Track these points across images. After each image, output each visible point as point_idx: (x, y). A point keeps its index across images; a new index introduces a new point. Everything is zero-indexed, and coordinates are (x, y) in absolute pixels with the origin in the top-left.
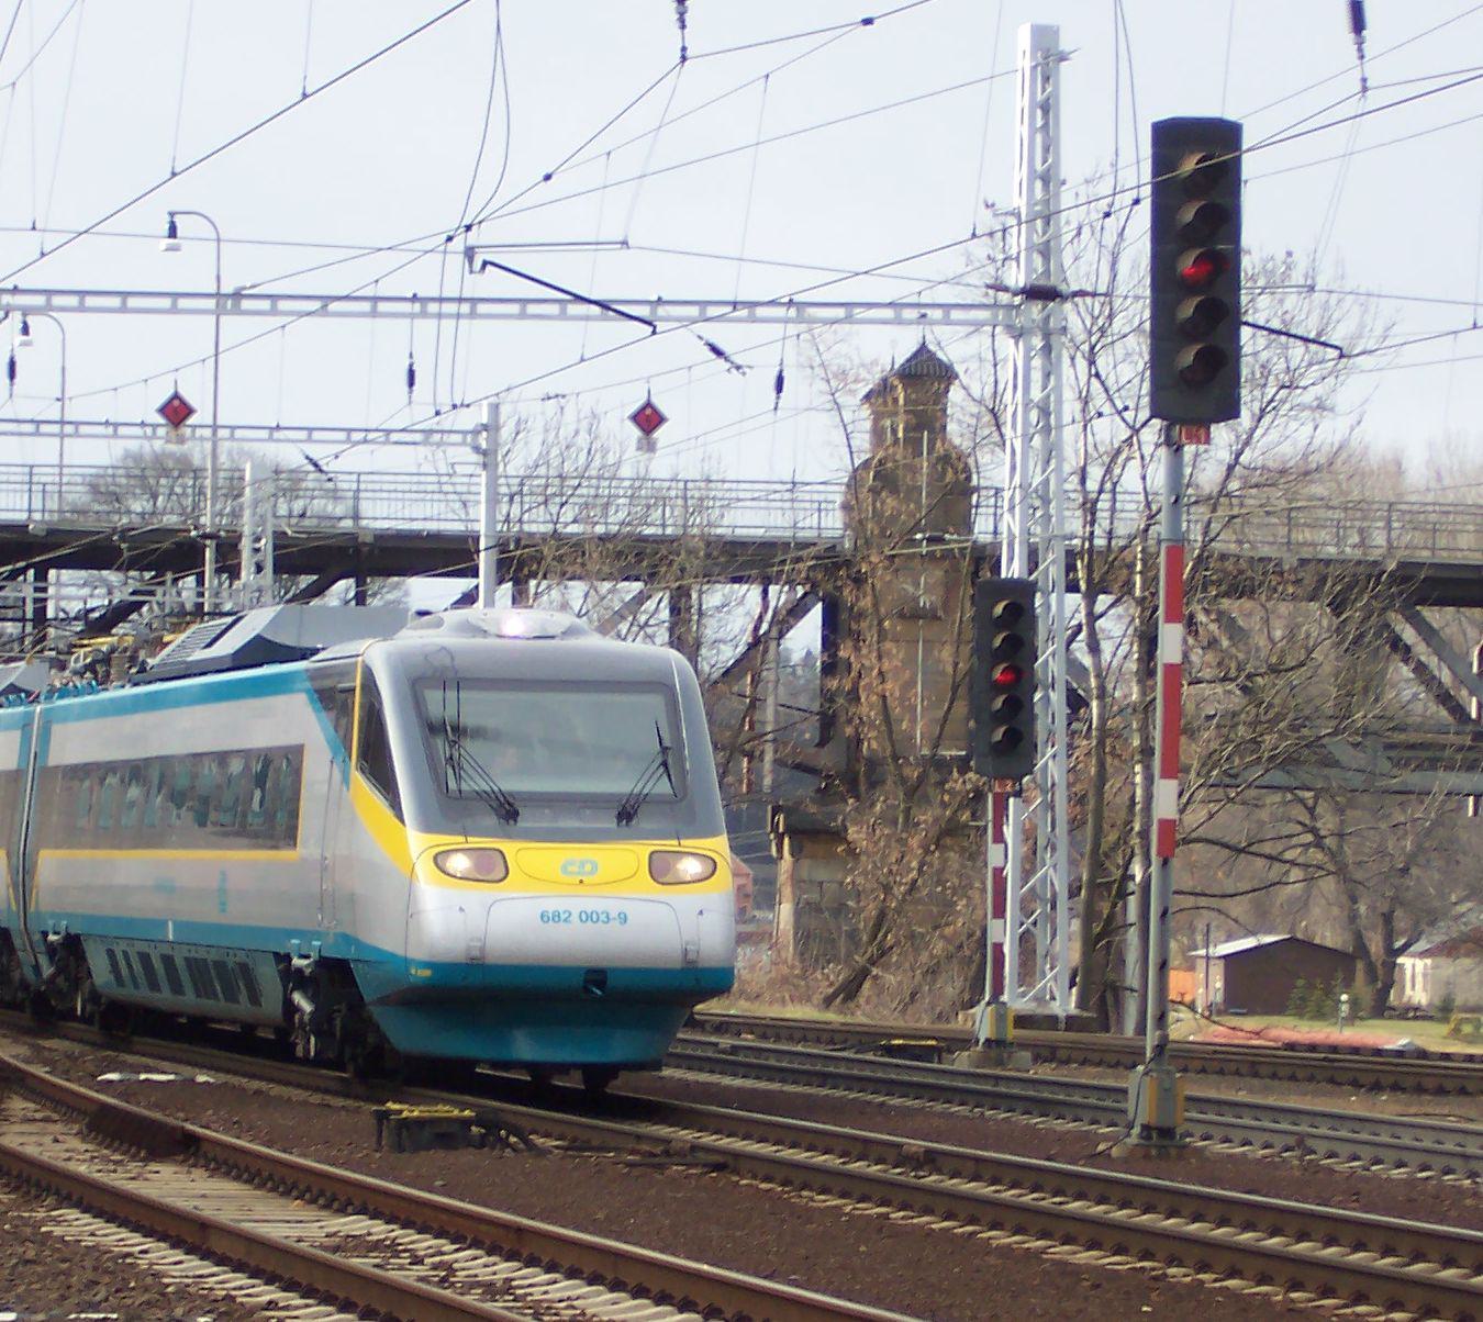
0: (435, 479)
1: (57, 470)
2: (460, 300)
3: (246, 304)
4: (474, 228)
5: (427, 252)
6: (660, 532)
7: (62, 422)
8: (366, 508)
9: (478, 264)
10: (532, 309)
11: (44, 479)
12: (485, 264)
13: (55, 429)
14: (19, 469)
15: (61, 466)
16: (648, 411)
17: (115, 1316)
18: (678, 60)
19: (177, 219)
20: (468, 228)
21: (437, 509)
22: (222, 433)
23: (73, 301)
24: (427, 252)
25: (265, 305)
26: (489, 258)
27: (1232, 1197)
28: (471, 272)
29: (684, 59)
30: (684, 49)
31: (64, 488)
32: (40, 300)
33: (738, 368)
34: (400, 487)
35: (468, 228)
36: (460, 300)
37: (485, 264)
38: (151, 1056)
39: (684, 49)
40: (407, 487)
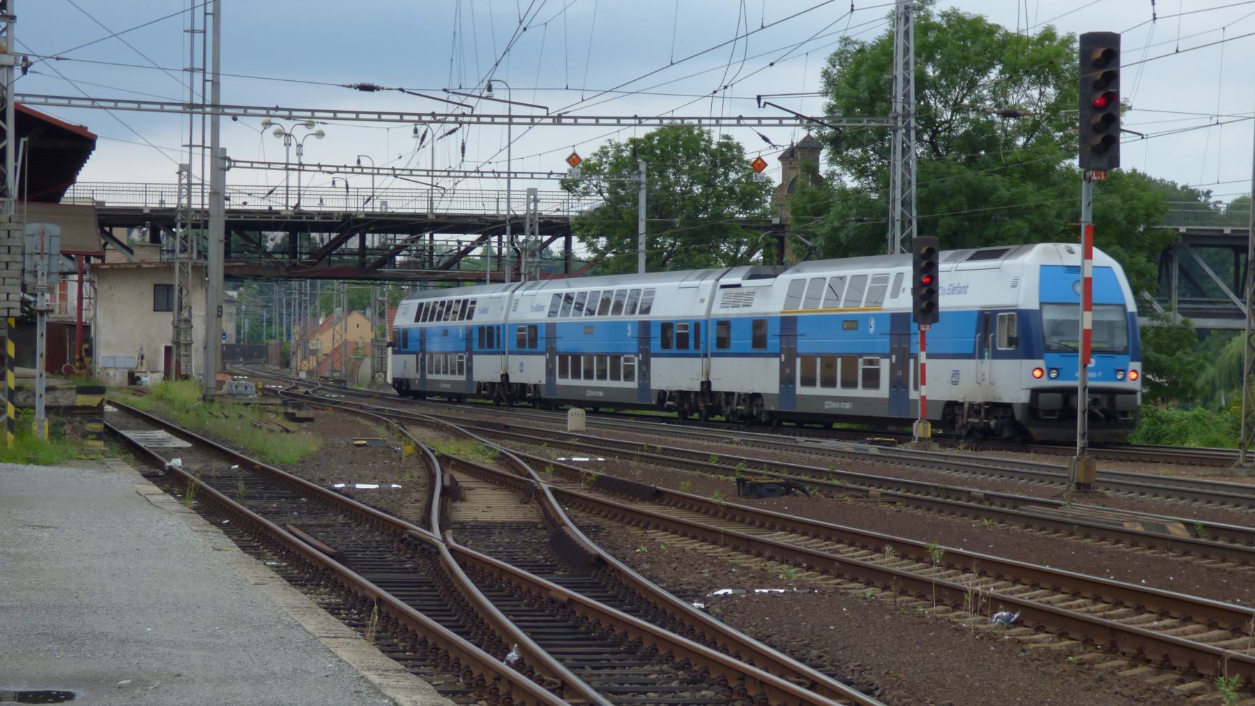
0: (480, 192)
1: (297, 189)
2: (711, 118)
3: (564, 121)
4: (729, 88)
5: (159, 68)
6: (371, 210)
7: (373, 168)
8: (390, 204)
9: (762, 105)
10: (785, 122)
11: (363, 194)
12: (765, 103)
13: (370, 171)
14: (493, 192)
15: (373, 189)
16: (574, 157)
17: (782, 591)
18: (850, 10)
19: (492, 83)
20: (726, 87)
21: (473, 205)
22: (512, 175)
23: (489, 120)
24: (159, 68)
25: (572, 121)
26: (767, 101)
27: (1183, 597)
28: (759, 107)
29: (852, 10)
30: (852, 6)
31: (345, 193)
32: (242, 111)
33: (774, 146)
34: (401, 194)
35: (726, 87)
36: (711, 118)
37: (765, 103)
38: (567, 468)
39: (852, 6)
40: (519, 197)
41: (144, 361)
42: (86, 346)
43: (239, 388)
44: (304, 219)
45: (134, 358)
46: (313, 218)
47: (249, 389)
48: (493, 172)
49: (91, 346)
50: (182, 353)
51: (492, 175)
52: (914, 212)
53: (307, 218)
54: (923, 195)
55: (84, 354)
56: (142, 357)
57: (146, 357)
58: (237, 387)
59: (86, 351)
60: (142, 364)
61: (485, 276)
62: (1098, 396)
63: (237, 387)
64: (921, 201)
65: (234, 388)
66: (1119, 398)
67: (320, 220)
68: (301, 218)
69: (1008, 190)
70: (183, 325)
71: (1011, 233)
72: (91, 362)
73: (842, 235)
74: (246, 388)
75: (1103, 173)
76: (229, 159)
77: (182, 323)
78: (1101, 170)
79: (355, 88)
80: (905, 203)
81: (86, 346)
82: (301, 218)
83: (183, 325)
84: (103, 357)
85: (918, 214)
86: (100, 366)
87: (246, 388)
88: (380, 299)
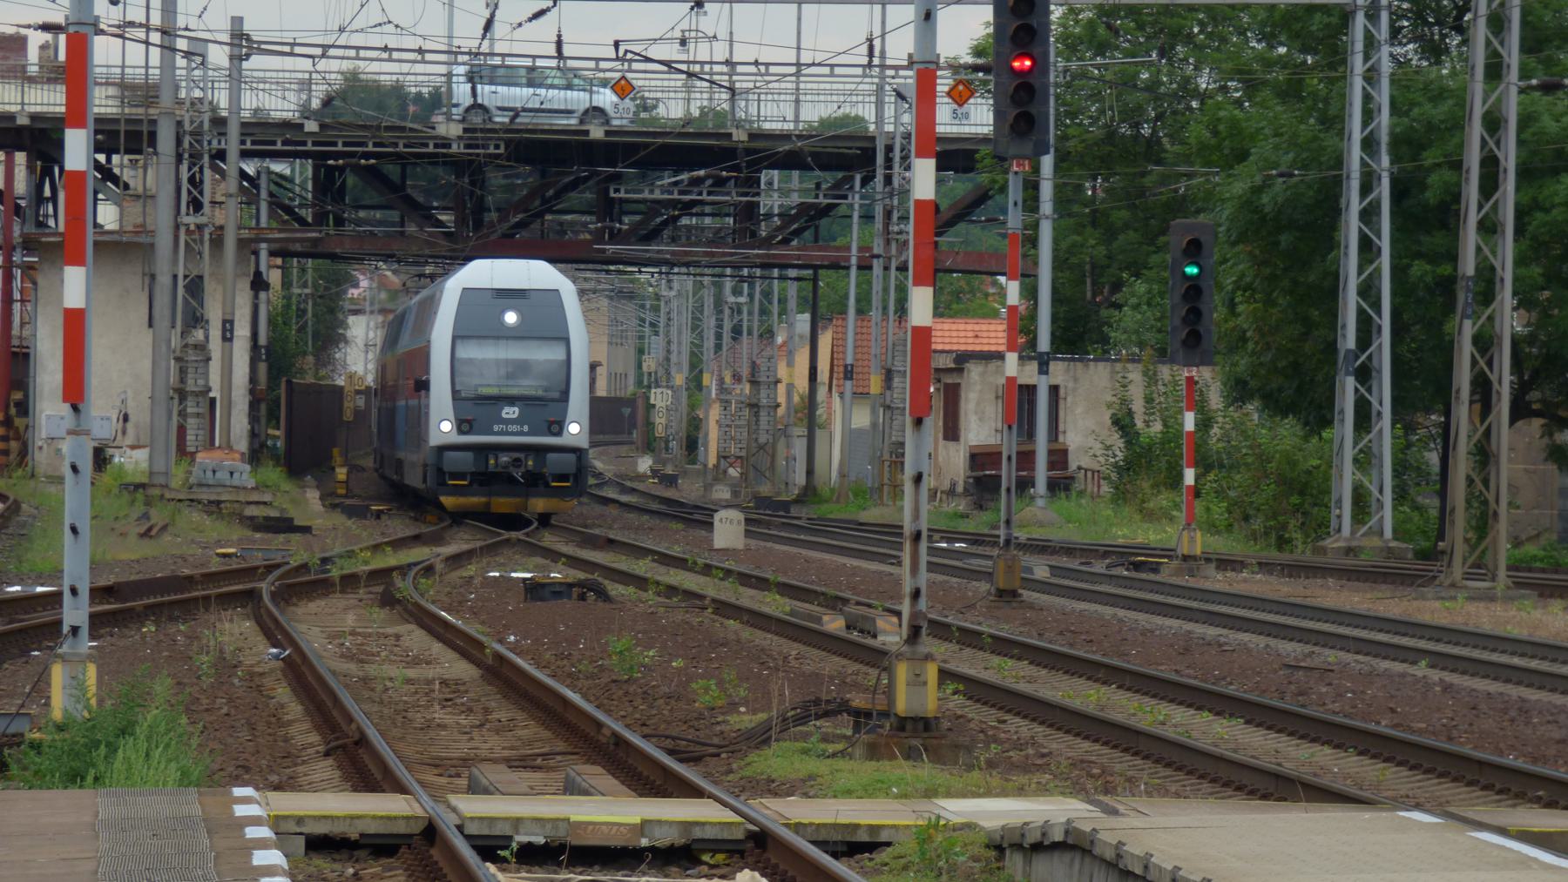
26: (629, 48)
41: (129, 425)
42: (18, 396)
43: (218, 475)
44: (431, 149)
45: (108, 419)
46: (449, 146)
47: (236, 475)
48: (756, 63)
49: (26, 396)
50: (189, 410)
51: (753, 69)
52: (1385, 161)
53: (436, 146)
54: (1398, 130)
55: (13, 411)
56: (126, 418)
57: (131, 417)
58: (214, 472)
59: (18, 404)
60: (124, 432)
61: (848, 259)
62: (521, 456)
63: (214, 472)
64: (1396, 142)
65: (209, 474)
66: (551, 456)
67: (462, 150)
68: (426, 145)
69: (1558, 121)
70: (192, 356)
71: (1557, 200)
72: (27, 427)
73: (1265, 199)
74: (232, 473)
75: (1027, 162)
76: (248, 38)
77: (190, 352)
78: (1025, 157)
79: (35, 29)
80: (1369, 144)
81: (18, 396)
82: (426, 145)
83: (192, 356)
84: (49, 417)
85: (1392, 163)
86: (44, 436)
87: (232, 473)
88: (731, 299)
